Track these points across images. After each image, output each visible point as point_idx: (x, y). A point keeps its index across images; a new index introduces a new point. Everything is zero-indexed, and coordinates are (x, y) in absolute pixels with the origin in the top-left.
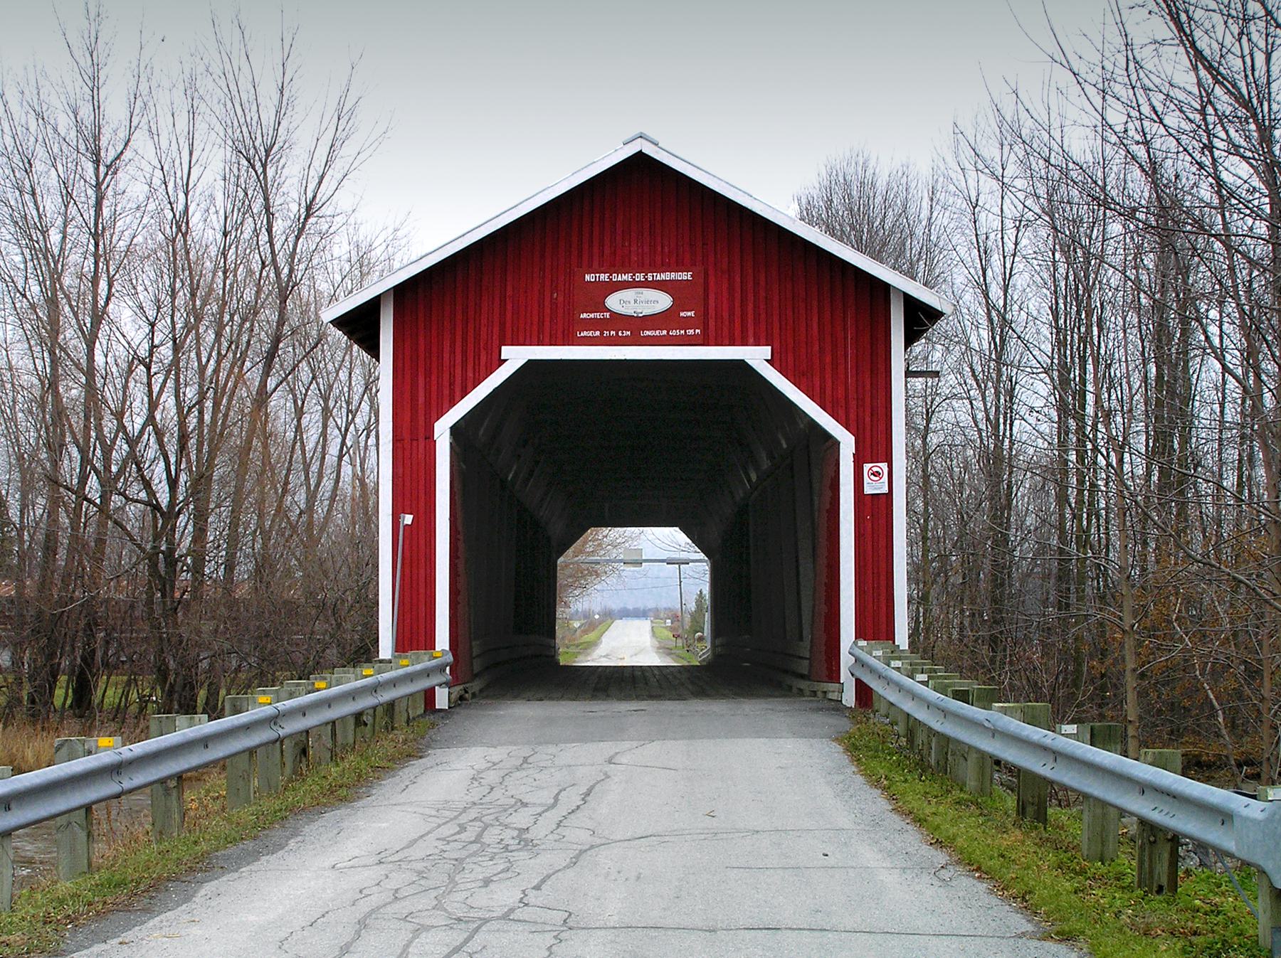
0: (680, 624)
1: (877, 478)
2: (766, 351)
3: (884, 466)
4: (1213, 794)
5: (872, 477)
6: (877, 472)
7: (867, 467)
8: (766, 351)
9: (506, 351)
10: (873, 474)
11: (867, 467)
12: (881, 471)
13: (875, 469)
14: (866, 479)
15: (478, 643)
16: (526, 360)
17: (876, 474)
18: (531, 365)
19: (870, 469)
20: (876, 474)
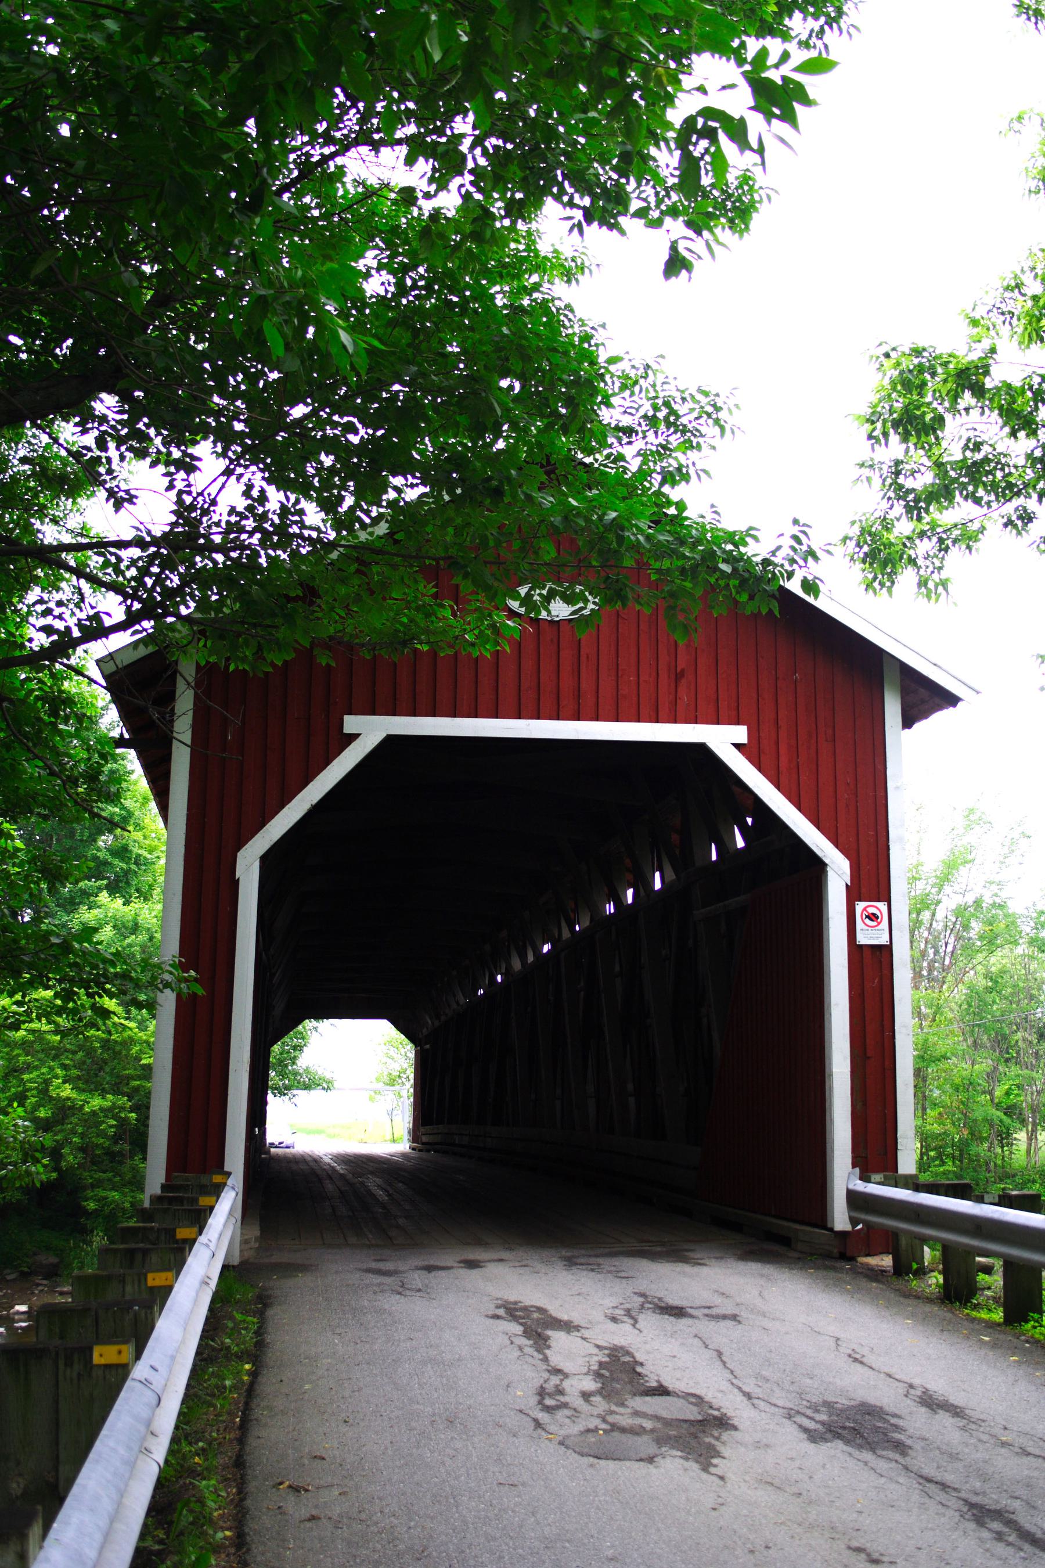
0: (901, 480)
1: (875, 923)
2: (740, 733)
3: (883, 906)
4: (1008, 1214)
5: (867, 921)
6: (874, 914)
7: (860, 906)
8: (740, 733)
9: (351, 723)
10: (867, 917)
11: (860, 906)
12: (879, 914)
13: (871, 910)
14: (859, 924)
15: (221, 513)
16: (257, 865)
17: (873, 917)
18: (391, 742)
19: (879, 924)
20: (873, 917)
